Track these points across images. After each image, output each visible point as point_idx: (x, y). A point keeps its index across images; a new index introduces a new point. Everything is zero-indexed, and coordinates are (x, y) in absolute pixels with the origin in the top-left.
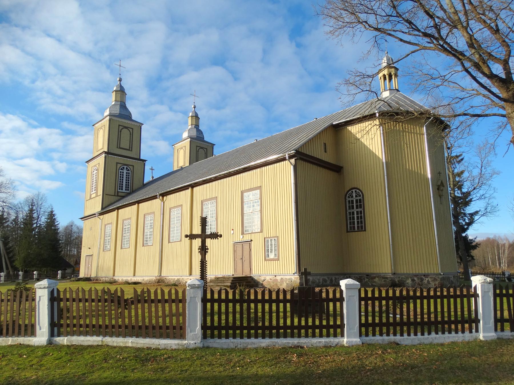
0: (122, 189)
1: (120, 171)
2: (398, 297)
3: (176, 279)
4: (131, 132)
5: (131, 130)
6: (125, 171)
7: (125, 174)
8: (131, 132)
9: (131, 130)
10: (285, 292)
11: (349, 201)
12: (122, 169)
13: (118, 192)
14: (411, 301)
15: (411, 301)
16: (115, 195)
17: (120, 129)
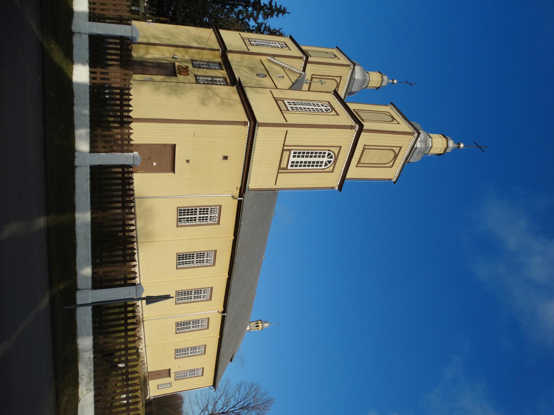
0: (294, 157)
1: (327, 152)
3: (141, 337)
7: (320, 159)
10: (134, 311)
12: (329, 154)
13: (290, 151)
14: (126, 205)
15: (126, 205)
16: (284, 145)
17: (336, 78)
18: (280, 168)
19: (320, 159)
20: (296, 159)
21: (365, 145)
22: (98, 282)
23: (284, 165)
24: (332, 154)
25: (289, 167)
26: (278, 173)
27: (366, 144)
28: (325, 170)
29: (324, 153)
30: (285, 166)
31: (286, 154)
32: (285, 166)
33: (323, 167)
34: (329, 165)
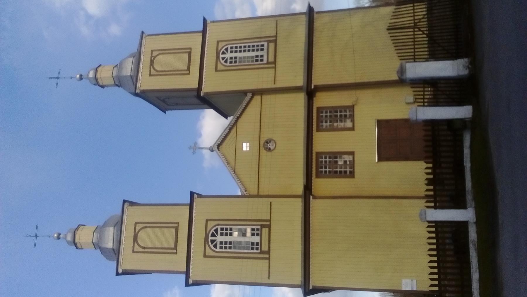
0: (262, 56)
2: (433, 165)
4: (142, 226)
5: (139, 227)
6: (228, 55)
7: (234, 55)
8: (142, 226)
9: (139, 227)
11: (221, 248)
12: (226, 62)
17: (155, 73)
18: (275, 42)
19: (234, 55)
20: (259, 53)
21: (176, 253)
22: (463, 226)
23: (272, 45)
24: (211, 246)
25: (266, 44)
26: (276, 36)
27: (188, 76)
28: (217, 223)
29: (231, 62)
30: (264, 229)
31: (271, 59)
32: (264, 229)
33: (229, 46)
34: (223, 49)
